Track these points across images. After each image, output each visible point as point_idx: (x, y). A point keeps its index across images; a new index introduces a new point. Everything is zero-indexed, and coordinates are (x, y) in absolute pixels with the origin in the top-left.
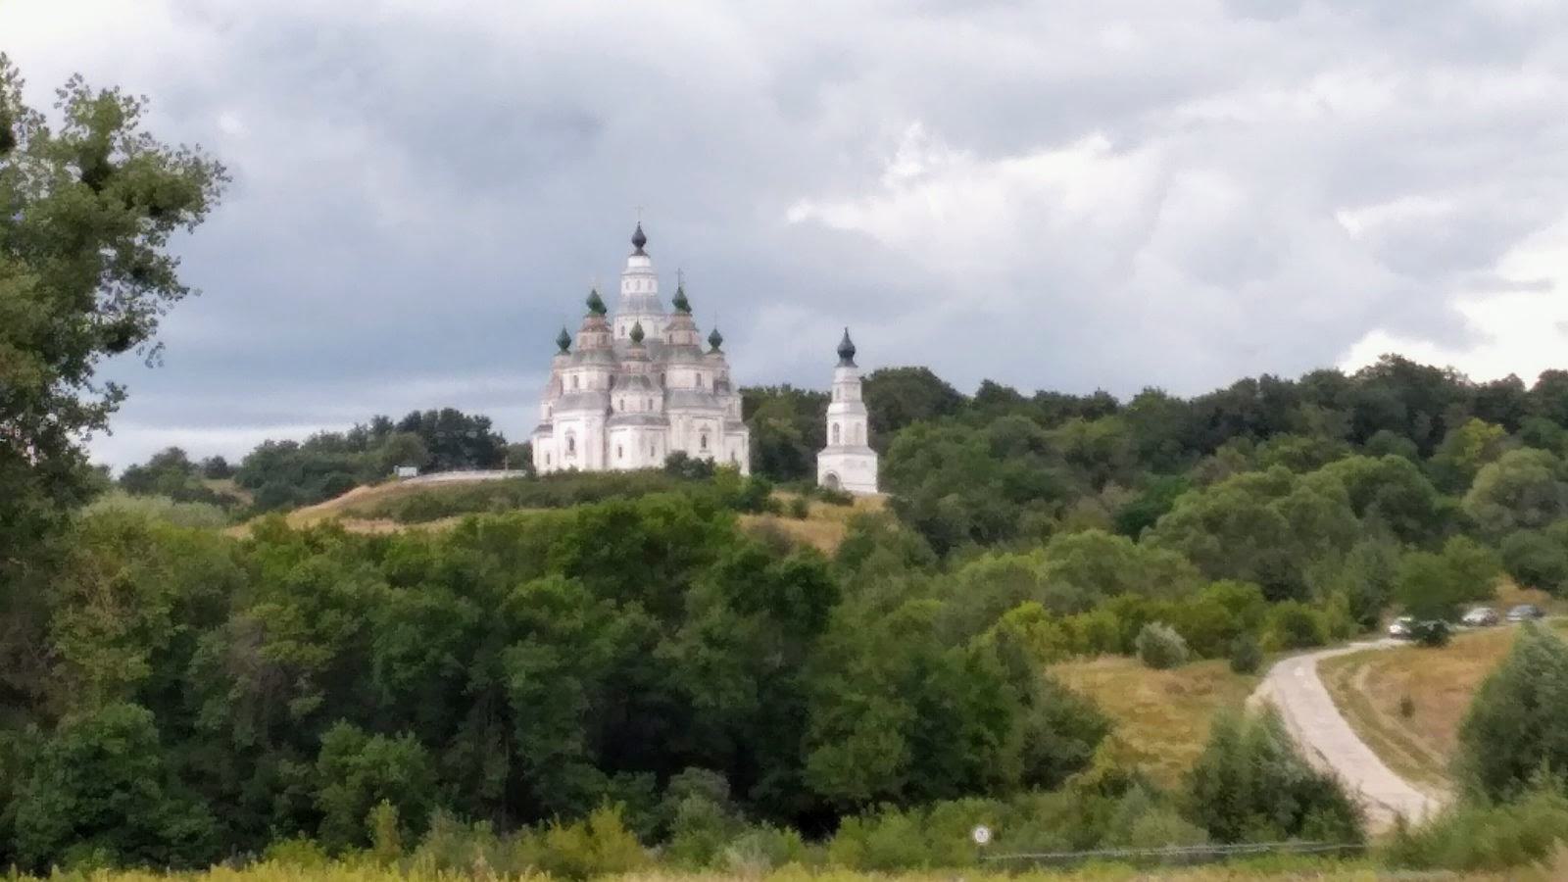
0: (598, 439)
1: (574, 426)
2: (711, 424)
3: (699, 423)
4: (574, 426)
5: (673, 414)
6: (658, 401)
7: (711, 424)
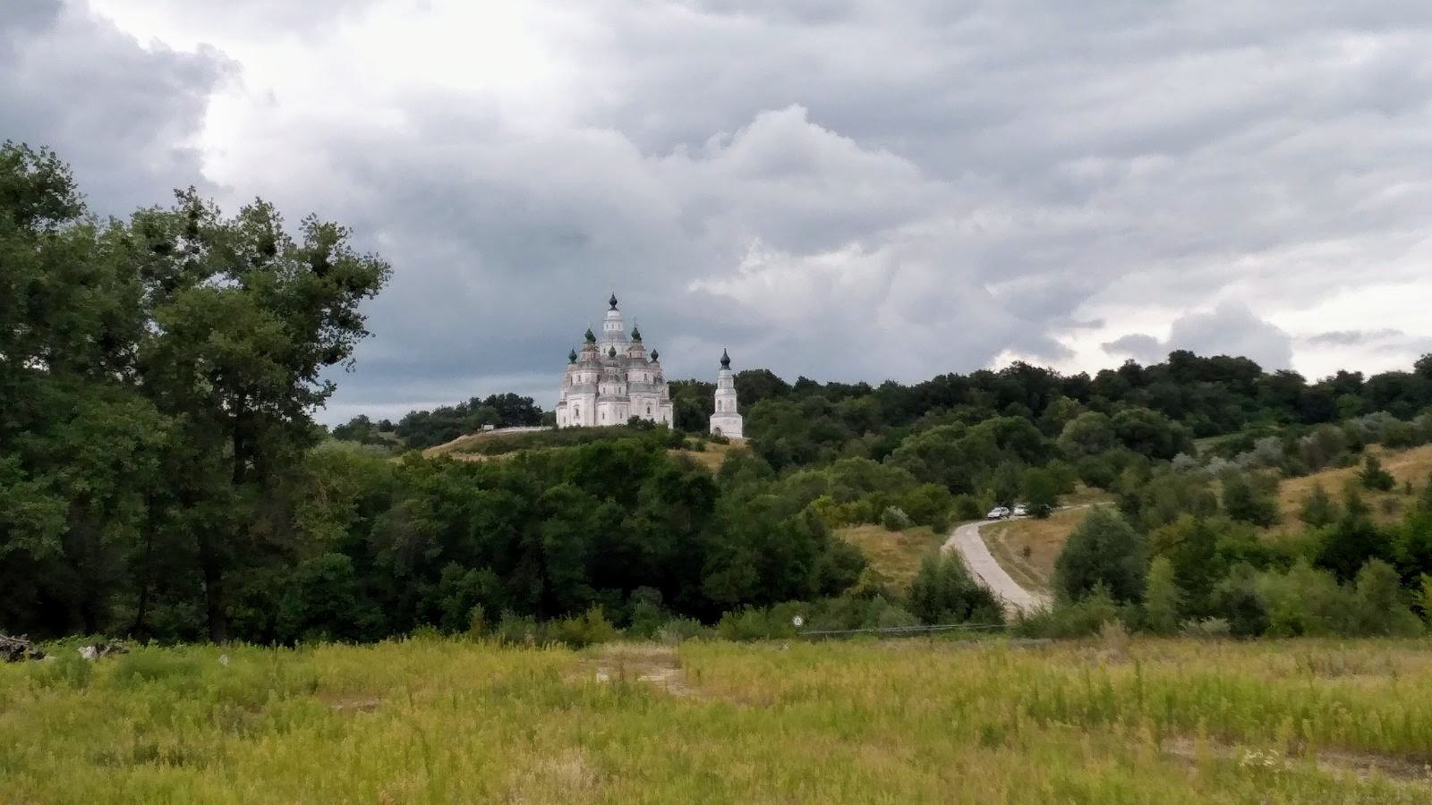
0: (591, 410)
1: (579, 402)
2: (653, 401)
3: (646, 400)
4: (579, 402)
5: (632, 396)
6: (624, 389)
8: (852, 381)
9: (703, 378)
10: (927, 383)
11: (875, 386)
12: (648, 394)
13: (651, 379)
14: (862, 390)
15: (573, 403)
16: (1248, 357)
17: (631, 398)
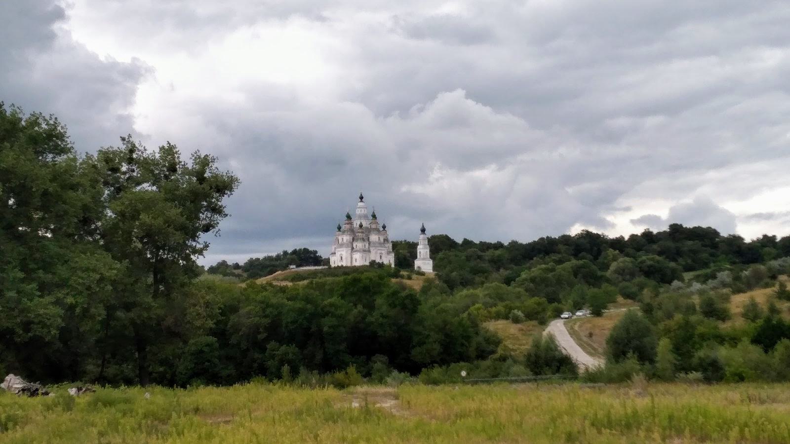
1: (342, 253)
2: (383, 252)
5: (372, 249)
7: (383, 252)
8: (493, 241)
9: (411, 240)
10: (535, 241)
11: (506, 244)
12: (380, 248)
13: (382, 240)
14: (499, 246)
15: (339, 253)
16: (713, 227)
17: (372, 250)
